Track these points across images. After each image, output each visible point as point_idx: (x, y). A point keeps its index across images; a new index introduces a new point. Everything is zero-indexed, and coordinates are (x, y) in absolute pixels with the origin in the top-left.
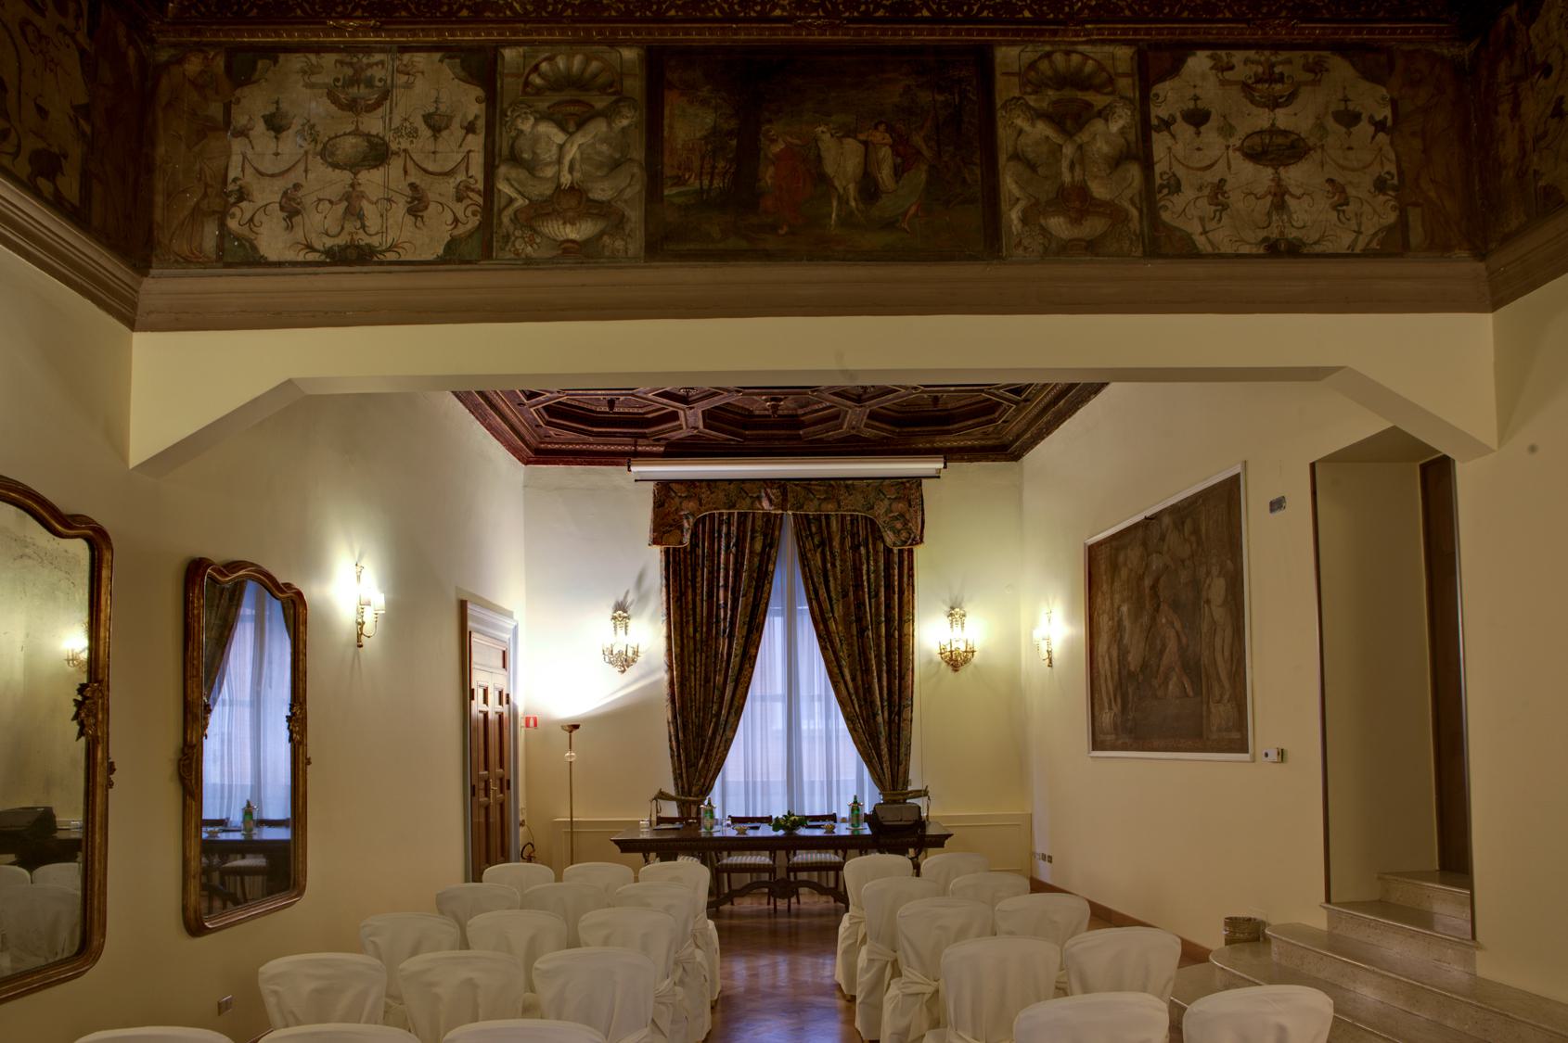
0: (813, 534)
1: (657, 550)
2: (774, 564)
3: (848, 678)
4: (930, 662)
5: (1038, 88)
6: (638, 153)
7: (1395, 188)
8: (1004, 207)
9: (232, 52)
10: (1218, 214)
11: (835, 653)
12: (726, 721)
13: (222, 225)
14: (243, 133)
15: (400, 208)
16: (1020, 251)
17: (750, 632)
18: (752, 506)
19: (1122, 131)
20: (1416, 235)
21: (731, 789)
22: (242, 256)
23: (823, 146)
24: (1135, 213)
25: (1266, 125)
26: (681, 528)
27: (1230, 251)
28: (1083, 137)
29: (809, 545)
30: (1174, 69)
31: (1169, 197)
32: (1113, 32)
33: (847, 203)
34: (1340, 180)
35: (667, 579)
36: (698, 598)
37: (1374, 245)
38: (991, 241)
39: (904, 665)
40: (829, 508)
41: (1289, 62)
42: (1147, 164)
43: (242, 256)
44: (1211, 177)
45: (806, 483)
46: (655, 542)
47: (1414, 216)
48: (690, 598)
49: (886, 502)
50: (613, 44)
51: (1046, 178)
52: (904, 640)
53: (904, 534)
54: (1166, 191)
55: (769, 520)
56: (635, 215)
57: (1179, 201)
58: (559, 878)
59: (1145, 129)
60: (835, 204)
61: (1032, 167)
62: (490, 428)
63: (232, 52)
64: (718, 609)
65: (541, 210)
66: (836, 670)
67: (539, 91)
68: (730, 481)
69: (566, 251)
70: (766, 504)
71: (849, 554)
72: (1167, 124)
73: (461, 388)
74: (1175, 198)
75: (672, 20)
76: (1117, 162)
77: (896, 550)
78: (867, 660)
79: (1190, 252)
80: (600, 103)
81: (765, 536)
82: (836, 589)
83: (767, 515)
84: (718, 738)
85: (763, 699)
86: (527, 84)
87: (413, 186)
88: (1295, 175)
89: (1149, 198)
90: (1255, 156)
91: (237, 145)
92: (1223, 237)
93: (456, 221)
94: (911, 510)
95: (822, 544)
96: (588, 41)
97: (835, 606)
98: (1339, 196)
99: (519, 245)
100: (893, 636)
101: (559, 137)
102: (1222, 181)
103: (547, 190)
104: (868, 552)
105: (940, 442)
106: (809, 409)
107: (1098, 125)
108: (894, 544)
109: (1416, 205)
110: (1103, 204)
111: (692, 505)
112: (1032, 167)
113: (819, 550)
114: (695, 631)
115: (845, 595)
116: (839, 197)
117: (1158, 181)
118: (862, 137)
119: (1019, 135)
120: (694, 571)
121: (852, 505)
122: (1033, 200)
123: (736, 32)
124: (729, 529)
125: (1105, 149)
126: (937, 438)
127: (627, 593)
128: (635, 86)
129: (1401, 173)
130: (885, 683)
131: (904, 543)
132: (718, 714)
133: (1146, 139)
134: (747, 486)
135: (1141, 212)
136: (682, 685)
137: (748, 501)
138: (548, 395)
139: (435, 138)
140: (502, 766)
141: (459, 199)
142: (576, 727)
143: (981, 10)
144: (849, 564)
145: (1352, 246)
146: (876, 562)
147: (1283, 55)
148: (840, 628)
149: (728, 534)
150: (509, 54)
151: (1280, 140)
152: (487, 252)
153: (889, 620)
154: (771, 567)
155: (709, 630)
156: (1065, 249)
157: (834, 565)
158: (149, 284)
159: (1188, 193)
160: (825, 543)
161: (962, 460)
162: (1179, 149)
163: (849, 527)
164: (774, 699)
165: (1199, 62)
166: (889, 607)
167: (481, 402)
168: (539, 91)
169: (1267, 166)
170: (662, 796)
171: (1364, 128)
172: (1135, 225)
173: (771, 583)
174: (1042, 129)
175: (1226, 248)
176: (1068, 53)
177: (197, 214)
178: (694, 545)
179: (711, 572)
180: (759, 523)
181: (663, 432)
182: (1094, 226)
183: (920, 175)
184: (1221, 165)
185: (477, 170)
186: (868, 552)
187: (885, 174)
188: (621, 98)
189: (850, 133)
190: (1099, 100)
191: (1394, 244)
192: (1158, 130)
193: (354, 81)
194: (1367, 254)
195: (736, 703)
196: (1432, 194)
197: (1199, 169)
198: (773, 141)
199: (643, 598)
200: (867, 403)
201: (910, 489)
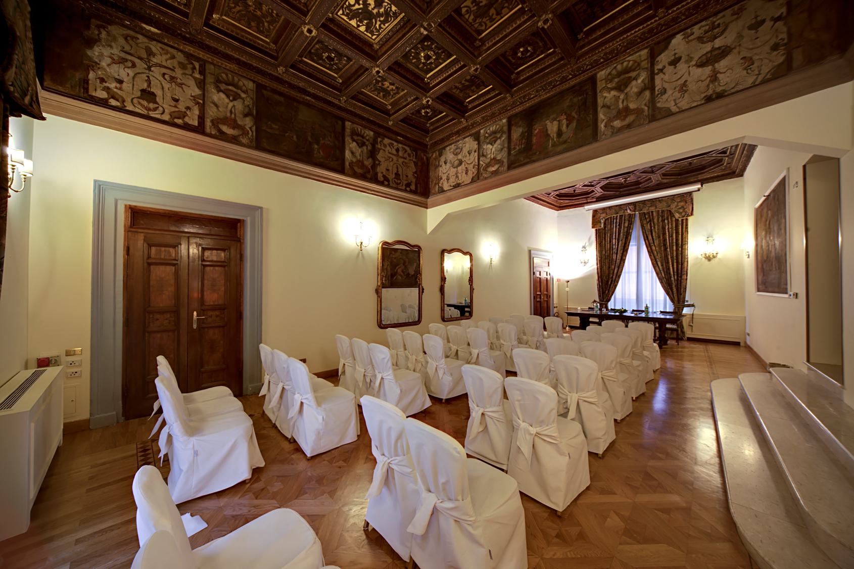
0: (646, 219)
2: (632, 230)
3: (659, 264)
5: (611, 81)
8: (599, 124)
9: (439, 150)
10: (683, 95)
11: (654, 257)
12: (615, 280)
13: (439, 185)
14: (441, 166)
16: (604, 136)
17: (623, 252)
18: (624, 212)
19: (643, 81)
21: (617, 301)
22: (442, 191)
23: (548, 126)
26: (600, 222)
27: (687, 107)
31: (661, 97)
32: (638, 48)
33: (554, 140)
35: (596, 238)
36: (606, 243)
39: (683, 259)
40: (652, 209)
43: (442, 191)
45: (644, 202)
48: (604, 243)
49: (676, 203)
51: (613, 109)
52: (683, 251)
53: (683, 214)
54: (659, 95)
55: (630, 216)
58: (627, 326)
60: (551, 141)
61: (609, 107)
63: (439, 150)
64: (613, 245)
65: (488, 165)
66: (655, 263)
67: (487, 137)
68: (616, 206)
69: (492, 174)
70: (629, 211)
71: (661, 223)
75: (510, 110)
77: (680, 219)
78: (668, 259)
79: (669, 113)
81: (629, 221)
82: (655, 235)
83: (630, 214)
84: (612, 285)
85: (629, 272)
86: (485, 137)
87: (466, 168)
91: (440, 169)
93: (473, 173)
94: (687, 204)
95: (650, 221)
96: (496, 121)
97: (655, 242)
99: (484, 175)
100: (679, 250)
104: (668, 222)
105: (700, 177)
106: (641, 178)
107: (634, 83)
108: (679, 218)
112: (609, 107)
113: (649, 224)
114: (605, 253)
116: (552, 139)
118: (558, 119)
119: (605, 99)
120: (605, 235)
121: (661, 206)
122: (609, 118)
123: (526, 105)
124: (616, 221)
126: (700, 176)
127: (586, 243)
130: (675, 266)
131: (684, 217)
132: (612, 278)
134: (622, 206)
135: (649, 107)
136: (601, 269)
137: (623, 211)
138: (667, 166)
139: (470, 156)
140: (547, 291)
141: (474, 168)
142: (568, 281)
143: (587, 67)
144: (661, 227)
146: (672, 224)
148: (657, 248)
149: (616, 222)
152: (478, 179)
154: (631, 231)
155: (610, 252)
156: (620, 130)
157: (654, 228)
158: (429, 200)
159: (669, 92)
160: (651, 221)
163: (661, 214)
164: (632, 272)
166: (677, 240)
169: (708, 66)
170: (595, 301)
173: (631, 236)
177: (435, 184)
178: (605, 227)
179: (610, 235)
180: (627, 217)
181: (592, 195)
183: (574, 124)
185: (476, 161)
186: (668, 222)
187: (564, 128)
189: (555, 119)
195: (618, 274)
197: (674, 82)
198: (536, 130)
199: (590, 244)
200: (657, 172)
201: (686, 197)
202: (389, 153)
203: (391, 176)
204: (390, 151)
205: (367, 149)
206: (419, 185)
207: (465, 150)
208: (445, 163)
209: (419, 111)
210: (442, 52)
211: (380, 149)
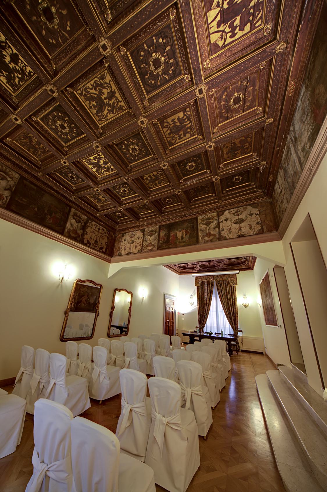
1: (196, 287)
3: (226, 308)
4: (241, 306)
5: (204, 221)
6: (157, 238)
7: (260, 223)
8: (199, 237)
14: (122, 242)
15: (134, 247)
17: (210, 300)
19: (215, 224)
20: (265, 230)
21: (208, 327)
24: (217, 235)
25: (237, 218)
28: (210, 226)
29: (218, 285)
30: (223, 214)
34: (250, 224)
37: (257, 233)
38: (197, 242)
40: (221, 279)
41: (241, 209)
42: (219, 228)
43: (120, 255)
44: (229, 228)
45: (217, 276)
46: (196, 285)
47: (264, 227)
50: (156, 226)
53: (234, 283)
56: (156, 245)
57: (224, 232)
59: (219, 223)
62: (171, 270)
63: (122, 234)
67: (148, 233)
68: (206, 276)
71: (225, 287)
72: (222, 222)
73: (164, 265)
74: (223, 232)
76: (215, 228)
79: (226, 239)
80: (154, 233)
83: (212, 281)
88: (242, 225)
89: (219, 233)
90: (235, 223)
91: (122, 243)
92: (231, 236)
95: (220, 285)
96: (153, 226)
98: (250, 226)
101: (150, 237)
102: (231, 228)
103: (148, 243)
105: (238, 268)
107: (212, 224)
109: (264, 225)
110: (213, 234)
111: (200, 280)
115: (225, 294)
117: (221, 230)
121: (225, 279)
125: (213, 227)
128: (158, 230)
129: (261, 221)
133: (219, 224)
145: (253, 234)
147: (240, 208)
150: (146, 229)
151: (240, 220)
153: (232, 298)
156: (207, 241)
159: (225, 230)
161: (243, 270)
162: (224, 225)
165: (226, 212)
166: (232, 296)
167: (168, 266)
168: (148, 233)
170: (197, 327)
171: (254, 215)
172: (217, 237)
174: (204, 226)
175: (231, 237)
176: (207, 215)
178: (201, 286)
180: (211, 282)
182: (211, 238)
183: (188, 235)
184: (231, 226)
185: (142, 243)
188: (156, 232)
190: (212, 221)
191: (261, 232)
192: (221, 223)
193: (132, 235)
194: (256, 234)
196: (268, 223)
199: (195, 294)
202: (94, 229)
203: (92, 242)
204: (95, 228)
205: (81, 224)
206: (108, 250)
207: (136, 236)
208: (125, 241)
209: (115, 213)
210: (132, 191)
211: (89, 226)
